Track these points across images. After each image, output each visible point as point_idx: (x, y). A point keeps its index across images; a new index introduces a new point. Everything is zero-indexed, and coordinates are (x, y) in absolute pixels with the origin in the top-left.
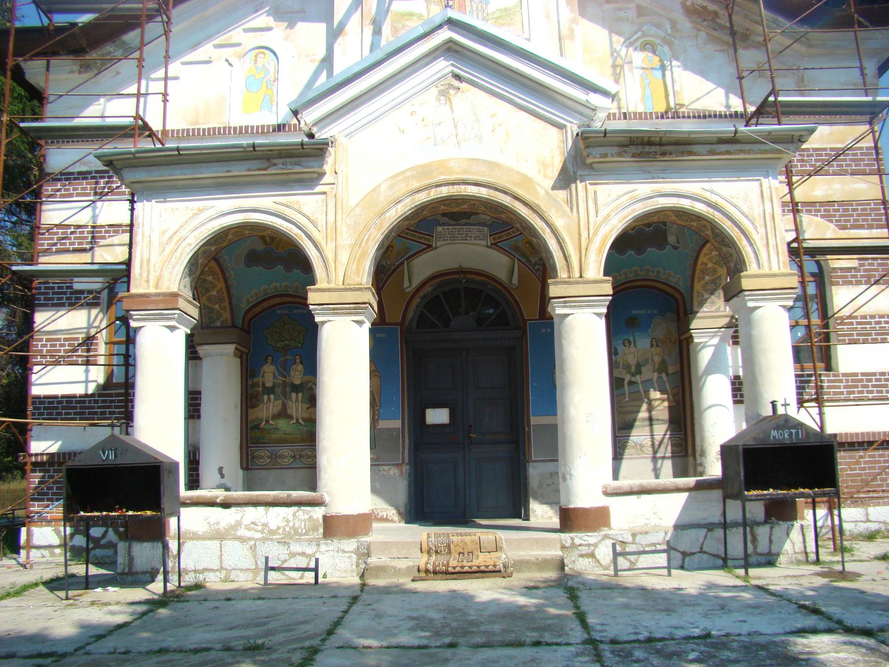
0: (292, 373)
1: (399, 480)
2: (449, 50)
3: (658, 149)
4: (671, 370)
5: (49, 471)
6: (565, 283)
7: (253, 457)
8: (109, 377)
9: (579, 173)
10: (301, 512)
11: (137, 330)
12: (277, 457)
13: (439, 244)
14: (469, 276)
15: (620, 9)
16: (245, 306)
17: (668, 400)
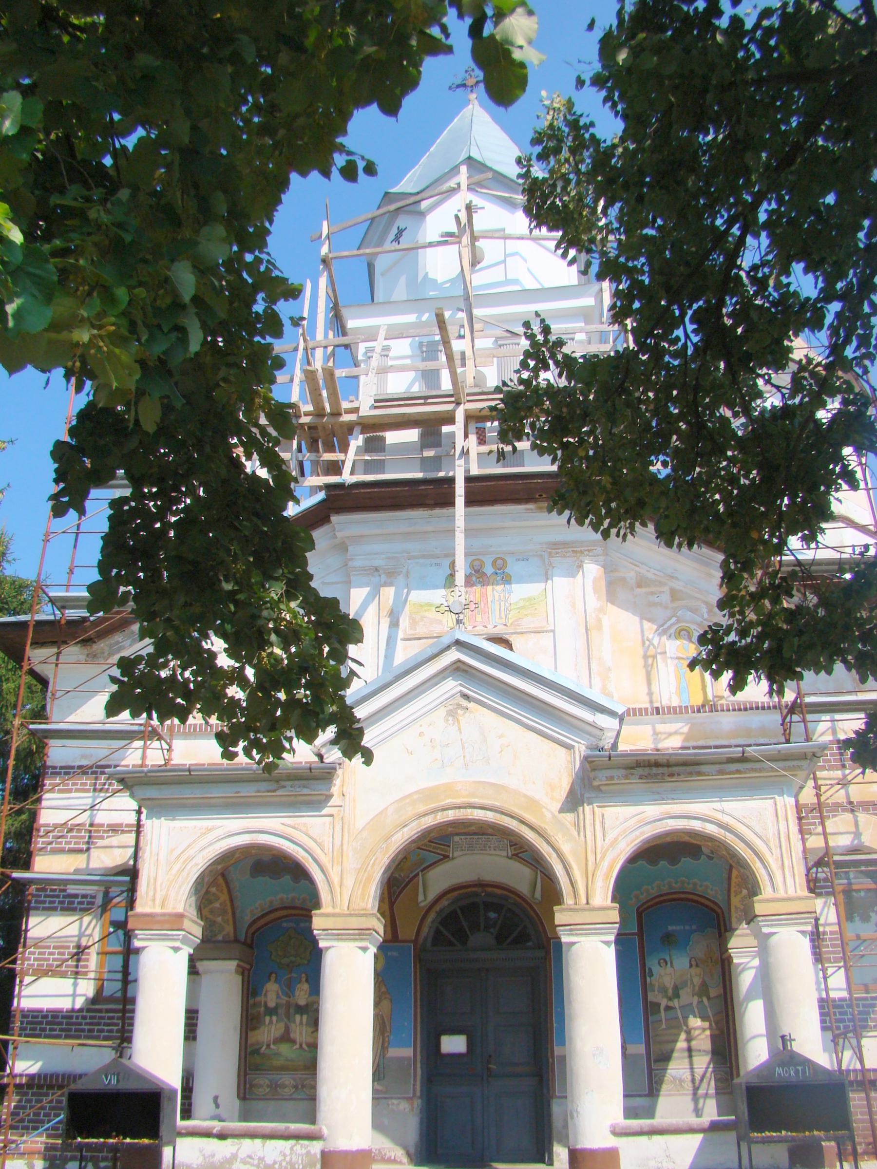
0: (297, 993)
1: (409, 1115)
2: (457, 669)
3: (665, 770)
4: (713, 993)
5: (26, 1094)
6: (571, 910)
7: (251, 1086)
8: (99, 991)
9: (586, 795)
10: (298, 1147)
11: (138, 951)
12: (277, 1086)
13: (456, 854)
14: (489, 889)
15: (652, 593)
16: (248, 918)
17: (710, 1028)
